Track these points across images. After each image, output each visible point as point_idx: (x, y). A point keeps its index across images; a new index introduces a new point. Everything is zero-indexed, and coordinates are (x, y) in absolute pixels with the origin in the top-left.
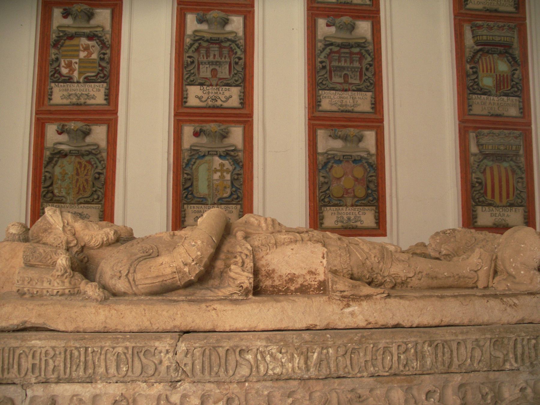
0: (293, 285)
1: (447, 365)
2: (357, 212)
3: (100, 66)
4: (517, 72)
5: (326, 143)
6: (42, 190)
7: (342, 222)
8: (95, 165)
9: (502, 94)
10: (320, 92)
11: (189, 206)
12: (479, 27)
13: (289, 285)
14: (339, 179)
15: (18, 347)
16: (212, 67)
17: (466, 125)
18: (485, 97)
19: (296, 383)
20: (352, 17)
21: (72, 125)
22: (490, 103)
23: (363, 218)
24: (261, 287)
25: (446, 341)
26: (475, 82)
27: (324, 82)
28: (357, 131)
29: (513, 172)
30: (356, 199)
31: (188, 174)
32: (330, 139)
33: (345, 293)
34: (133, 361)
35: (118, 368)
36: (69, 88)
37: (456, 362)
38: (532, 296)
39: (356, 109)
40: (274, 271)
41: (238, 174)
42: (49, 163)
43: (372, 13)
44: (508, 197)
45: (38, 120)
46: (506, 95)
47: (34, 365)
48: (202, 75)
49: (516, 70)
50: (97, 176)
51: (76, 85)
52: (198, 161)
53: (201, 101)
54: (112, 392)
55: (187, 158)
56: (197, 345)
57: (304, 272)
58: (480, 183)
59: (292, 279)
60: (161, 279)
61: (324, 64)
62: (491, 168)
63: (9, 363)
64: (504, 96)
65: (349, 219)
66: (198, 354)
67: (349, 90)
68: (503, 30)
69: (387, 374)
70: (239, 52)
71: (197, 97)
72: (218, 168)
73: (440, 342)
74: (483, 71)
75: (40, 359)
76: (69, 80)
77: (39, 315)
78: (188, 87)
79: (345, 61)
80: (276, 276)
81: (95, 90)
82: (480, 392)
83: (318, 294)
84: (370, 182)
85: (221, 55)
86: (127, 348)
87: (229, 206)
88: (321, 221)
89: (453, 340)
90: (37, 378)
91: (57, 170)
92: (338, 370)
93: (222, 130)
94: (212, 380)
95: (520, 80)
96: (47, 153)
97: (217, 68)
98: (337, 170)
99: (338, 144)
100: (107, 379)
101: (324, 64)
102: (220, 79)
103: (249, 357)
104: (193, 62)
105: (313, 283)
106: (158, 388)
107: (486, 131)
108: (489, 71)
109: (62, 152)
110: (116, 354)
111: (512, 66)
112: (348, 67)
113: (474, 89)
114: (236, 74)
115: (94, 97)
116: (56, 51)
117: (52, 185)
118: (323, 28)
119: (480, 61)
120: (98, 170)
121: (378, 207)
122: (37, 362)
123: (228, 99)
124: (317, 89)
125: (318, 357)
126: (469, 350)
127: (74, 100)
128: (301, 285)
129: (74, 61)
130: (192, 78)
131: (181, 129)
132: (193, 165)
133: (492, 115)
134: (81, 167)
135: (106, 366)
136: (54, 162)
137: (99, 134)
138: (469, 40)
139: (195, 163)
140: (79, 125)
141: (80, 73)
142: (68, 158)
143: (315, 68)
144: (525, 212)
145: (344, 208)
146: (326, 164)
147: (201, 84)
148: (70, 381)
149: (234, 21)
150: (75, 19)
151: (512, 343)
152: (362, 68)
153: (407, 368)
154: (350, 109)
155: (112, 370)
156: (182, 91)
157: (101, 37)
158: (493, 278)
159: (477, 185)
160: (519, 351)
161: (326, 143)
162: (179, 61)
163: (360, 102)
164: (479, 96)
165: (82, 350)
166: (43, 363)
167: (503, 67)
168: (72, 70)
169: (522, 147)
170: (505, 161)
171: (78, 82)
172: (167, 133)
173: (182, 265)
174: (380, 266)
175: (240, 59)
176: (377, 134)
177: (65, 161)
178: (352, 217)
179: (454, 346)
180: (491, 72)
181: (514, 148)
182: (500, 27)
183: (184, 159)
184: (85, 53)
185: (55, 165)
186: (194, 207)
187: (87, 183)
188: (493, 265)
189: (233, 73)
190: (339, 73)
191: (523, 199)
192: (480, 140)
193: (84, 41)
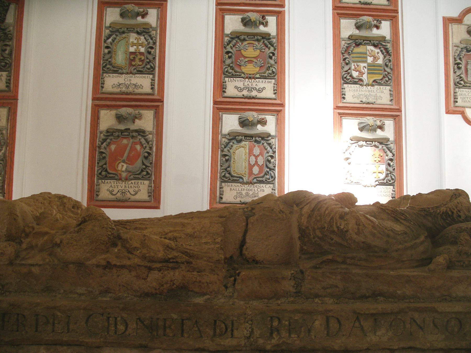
43: (391, 13)
76: (359, 82)
88: (97, 193)
127: (124, 89)
137: (146, 121)
168: (361, 73)
176: (277, 120)
193: (370, 48)
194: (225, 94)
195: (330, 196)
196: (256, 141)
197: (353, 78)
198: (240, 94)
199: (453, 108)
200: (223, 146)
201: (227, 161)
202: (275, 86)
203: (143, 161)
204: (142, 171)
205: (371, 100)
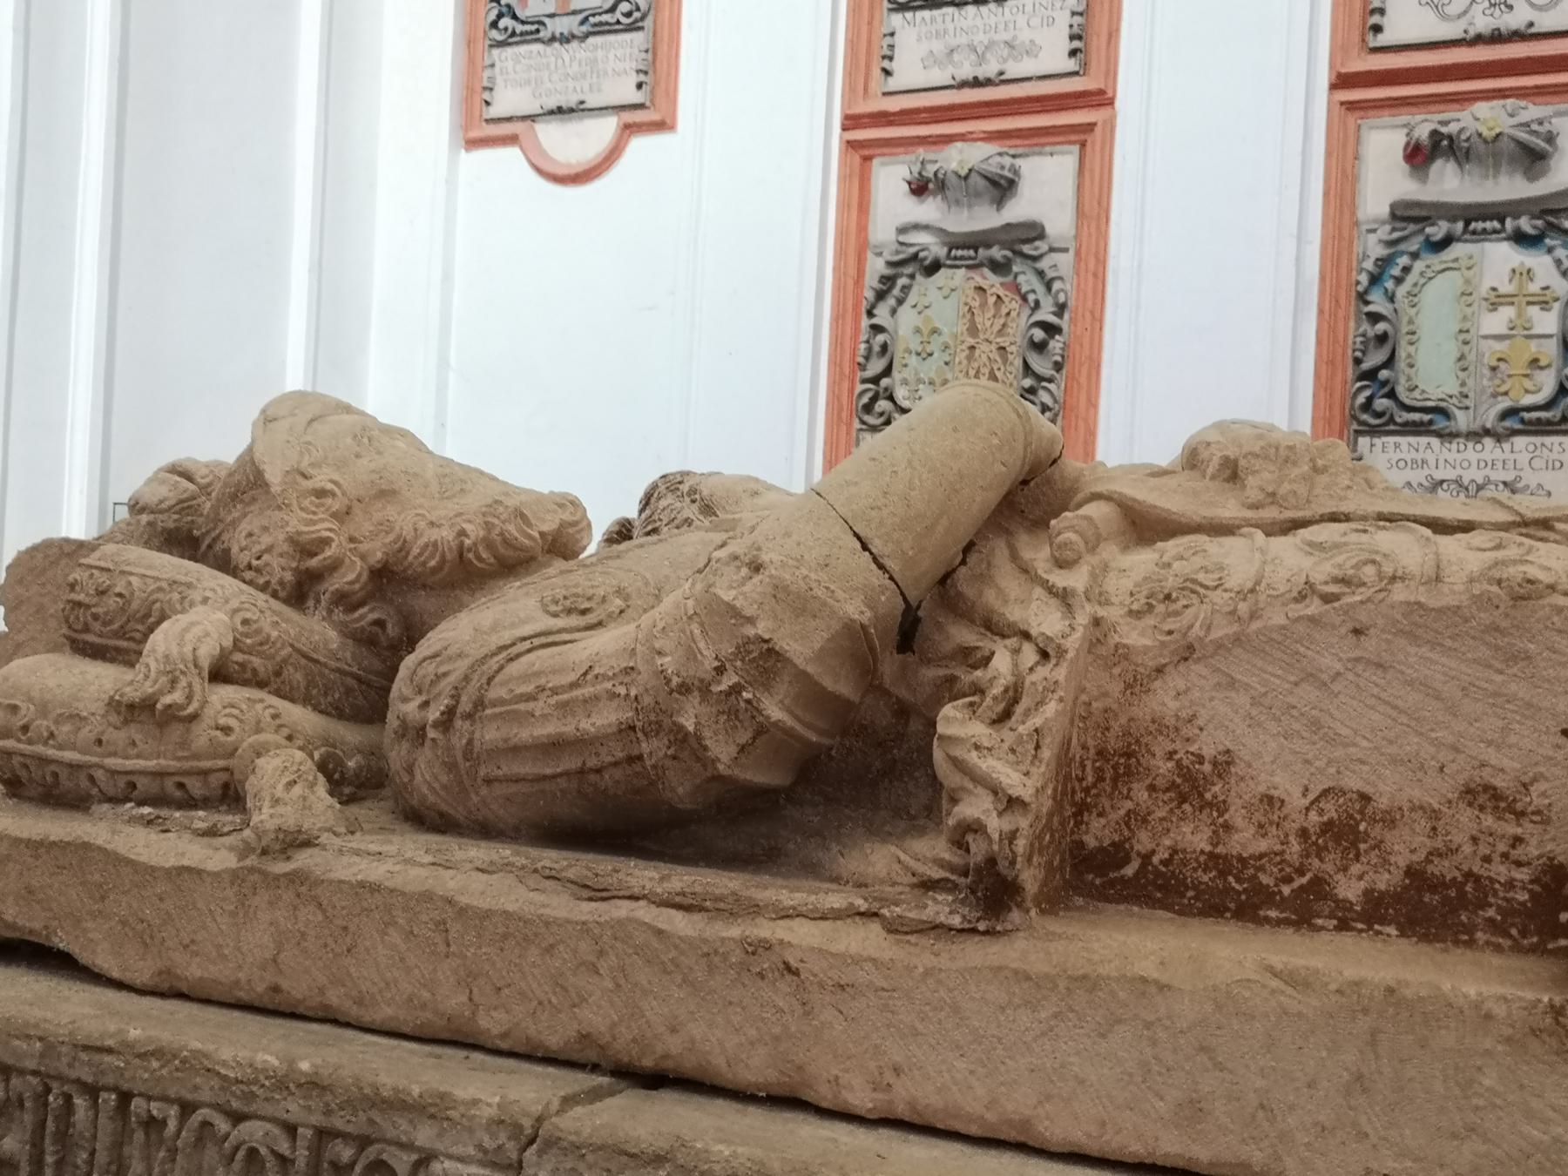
0: (1356, 869)
6: (860, 387)
8: (1031, 297)
11: (1378, 441)
13: (1327, 866)
24: (1146, 858)
31: (1375, 318)
36: (950, 27)
40: (1224, 764)
42: (881, 296)
50: (1039, 334)
52: (1419, 266)
53: (1445, 17)
59: (1347, 828)
60: (570, 763)
72: (1506, 288)
80: (1239, 797)
81: (1035, 22)
83: (1532, 950)
86: (291, 1130)
87: (1548, 440)
93: (1527, 125)
96: (876, 266)
105: (1500, 871)
109: (922, 255)
110: (241, 1154)
115: (1032, 50)
117: (887, 371)
120: (1045, 314)
128: (1410, 872)
132: (1399, 281)
134: (984, 304)
136: (896, 291)
139: (1406, 270)
172: (1299, 159)
174: (1072, 1059)
177: (927, 290)
183: (1365, 256)
185: (900, 302)
186: (1397, 446)
187: (1005, 360)
194: (1380, 36)
195: (552, 493)
198: (1452, 31)
199: (482, 126)
200: (1364, 279)
201: (1382, 339)
203: (1025, 362)
205: (989, 70)
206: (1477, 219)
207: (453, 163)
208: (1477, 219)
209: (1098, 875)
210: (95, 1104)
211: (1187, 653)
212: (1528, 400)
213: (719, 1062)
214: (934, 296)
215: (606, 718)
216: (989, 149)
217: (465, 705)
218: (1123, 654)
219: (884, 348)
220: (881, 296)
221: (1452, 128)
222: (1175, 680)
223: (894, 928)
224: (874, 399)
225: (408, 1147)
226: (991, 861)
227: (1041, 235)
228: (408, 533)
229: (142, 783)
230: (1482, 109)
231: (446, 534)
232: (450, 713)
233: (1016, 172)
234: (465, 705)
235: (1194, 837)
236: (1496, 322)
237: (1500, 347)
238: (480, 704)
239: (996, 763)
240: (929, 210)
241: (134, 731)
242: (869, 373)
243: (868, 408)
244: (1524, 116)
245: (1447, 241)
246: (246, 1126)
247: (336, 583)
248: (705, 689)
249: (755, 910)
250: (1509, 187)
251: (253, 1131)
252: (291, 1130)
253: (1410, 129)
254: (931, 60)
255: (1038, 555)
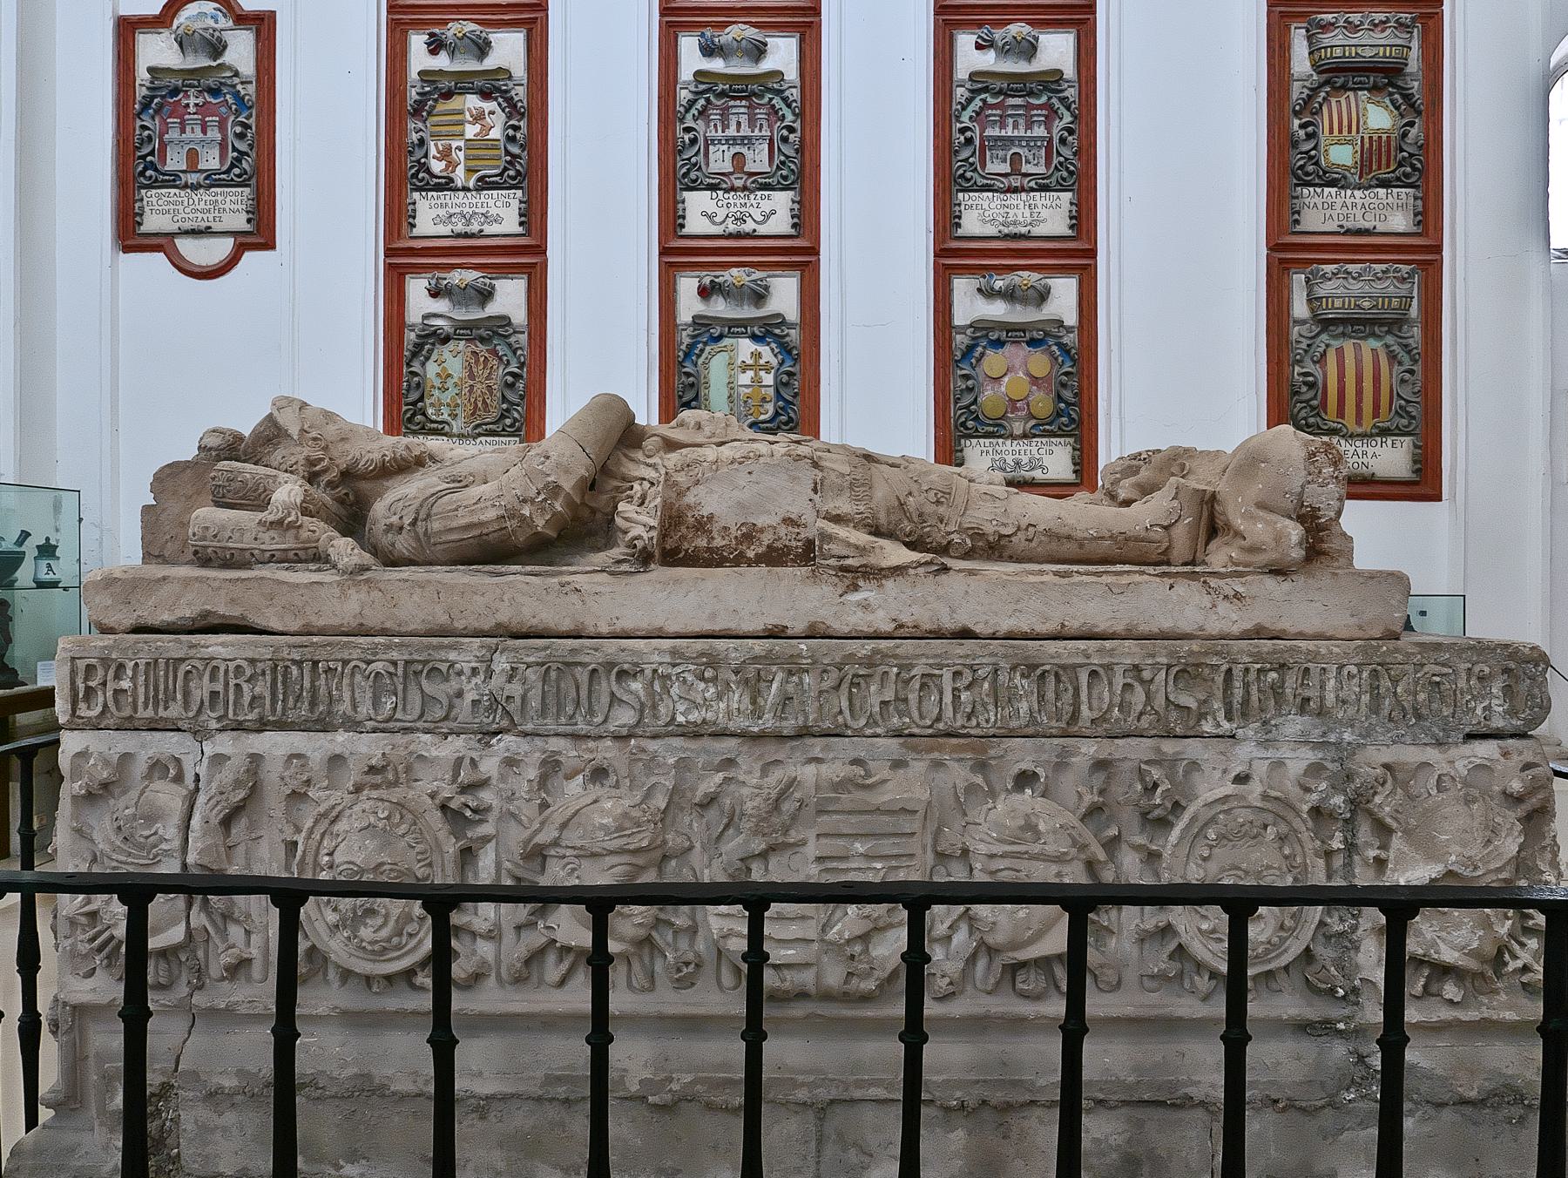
1: (1066, 717)
2: (1034, 450)
3: (508, 153)
4: (1414, 131)
5: (969, 305)
7: (1004, 470)
9: (1374, 182)
10: (960, 195)
12: (1327, 27)
14: (998, 379)
15: (183, 660)
16: (734, 150)
17: (1282, 255)
18: (1333, 190)
19: (732, 743)
20: (1030, 23)
21: (457, 277)
22: (1345, 205)
23: (1047, 461)
25: (1064, 667)
26: (1311, 158)
27: (968, 175)
28: (1035, 276)
29: (1392, 357)
30: (1033, 422)
31: (688, 375)
32: (979, 296)
33: (849, 562)
34: (405, 690)
35: (376, 703)
37: (1085, 712)
38: (1280, 578)
39: (1036, 231)
40: (711, 517)
41: (790, 374)
42: (414, 355)
44: (1376, 414)
45: (389, 268)
46: (1385, 184)
47: (214, 694)
48: (715, 167)
49: (1411, 124)
50: (510, 379)
51: (461, 194)
52: (708, 349)
53: (714, 223)
54: (364, 749)
55: (687, 341)
56: (532, 659)
57: (773, 520)
58: (1311, 386)
60: (476, 532)
61: (968, 134)
62: (1340, 352)
63: (166, 688)
64: (1378, 186)
65: (1018, 463)
66: (533, 677)
67: (1023, 190)
68: (1383, 31)
69: (930, 731)
70: (790, 117)
71: (705, 214)
72: (750, 362)
73: (1047, 667)
74: (1331, 131)
75: (227, 684)
76: (446, 185)
77: (232, 600)
78: (685, 194)
79: (1015, 126)
80: (716, 528)
82: (1142, 780)
84: (1064, 385)
85: (752, 124)
86: (395, 664)
89: (1081, 666)
90: (219, 719)
91: (432, 369)
92: (821, 717)
94: (561, 729)
95: (1420, 147)
96: (411, 337)
97: (744, 150)
98: (994, 361)
99: (997, 310)
100: (353, 725)
101: (968, 134)
102: (751, 174)
103: (636, 686)
104: (694, 141)
105: (794, 544)
106: (456, 746)
107: (1329, 268)
108: (1345, 129)
111: (1402, 116)
112: (1021, 139)
113: (1308, 174)
114: (783, 163)
115: (498, 220)
116: (420, 125)
117: (421, 399)
118: (970, 57)
119: (1325, 109)
121: (1079, 439)
122: (219, 687)
123: (767, 217)
124: (954, 189)
125: (780, 689)
126: (1118, 689)
127: (460, 228)
129: (455, 144)
130: (693, 175)
131: (675, 283)
132: (699, 356)
133: (1348, 232)
134: (477, 361)
135: (353, 699)
138: (1301, 62)
139: (702, 351)
140: (470, 276)
141: (470, 171)
142: (451, 345)
143: (951, 143)
144: (1416, 447)
145: (1008, 442)
146: (970, 349)
147: (713, 188)
148: (282, 726)
149: (778, 46)
150: (452, 54)
151: (1220, 679)
152: (1051, 139)
153: (974, 722)
154: (1024, 230)
155: (365, 709)
156: (676, 202)
157: (506, 91)
158: (1207, 544)
159: (1304, 389)
160: (1238, 693)
161: (969, 305)
162: (666, 139)
163: (1045, 213)
164: (1319, 190)
165: (307, 666)
166: (231, 690)
167: (1379, 118)
168: (452, 165)
169: (1415, 301)
170: (1373, 335)
171: (465, 189)
173: (517, 505)
175: (791, 130)
177: (445, 352)
178: (1025, 460)
179: (1084, 678)
180: (1350, 131)
181: (1395, 303)
182: (1376, 25)
184: (477, 128)
185: (427, 359)
188: (1205, 514)
189: (776, 162)
190: (1001, 153)
191: (1414, 418)
192: (1316, 288)
193: (473, 102)
196: (1032, 343)
197: (433, 176)
198: (718, 230)
199: (130, 235)
202: (796, 206)
204: (503, 417)
206: (735, 327)
207: (114, 261)
208: (735, 327)
209: (671, 557)
210: (301, 669)
211: (697, 483)
212: (762, 418)
213: (552, 625)
214: (447, 355)
215: (491, 514)
216: (475, 274)
217: (422, 515)
218: (676, 484)
219: (418, 385)
220: (414, 355)
221: (721, 280)
222: (694, 491)
223: (612, 574)
224: (414, 415)
225: (447, 661)
226: (645, 548)
227: (510, 324)
228: (358, 455)
229: (277, 554)
230: (734, 271)
231: (376, 456)
232: (416, 519)
233: (493, 287)
234: (422, 515)
235: (702, 542)
236: (746, 378)
237: (748, 391)
238: (429, 516)
239: (638, 520)
240: (441, 306)
241: (272, 533)
242: (410, 400)
243: (410, 420)
244: (754, 277)
245: (721, 337)
246: (373, 665)
247: (326, 478)
248: (532, 501)
249: (561, 573)
250: (748, 312)
251: (378, 666)
252: (395, 664)
253: (701, 279)
254: (437, 221)
255: (639, 455)
